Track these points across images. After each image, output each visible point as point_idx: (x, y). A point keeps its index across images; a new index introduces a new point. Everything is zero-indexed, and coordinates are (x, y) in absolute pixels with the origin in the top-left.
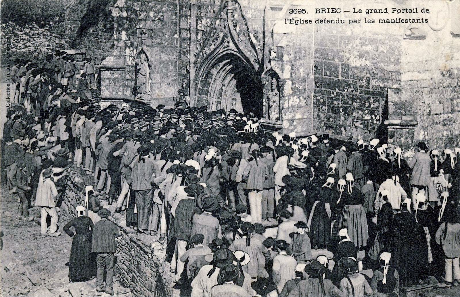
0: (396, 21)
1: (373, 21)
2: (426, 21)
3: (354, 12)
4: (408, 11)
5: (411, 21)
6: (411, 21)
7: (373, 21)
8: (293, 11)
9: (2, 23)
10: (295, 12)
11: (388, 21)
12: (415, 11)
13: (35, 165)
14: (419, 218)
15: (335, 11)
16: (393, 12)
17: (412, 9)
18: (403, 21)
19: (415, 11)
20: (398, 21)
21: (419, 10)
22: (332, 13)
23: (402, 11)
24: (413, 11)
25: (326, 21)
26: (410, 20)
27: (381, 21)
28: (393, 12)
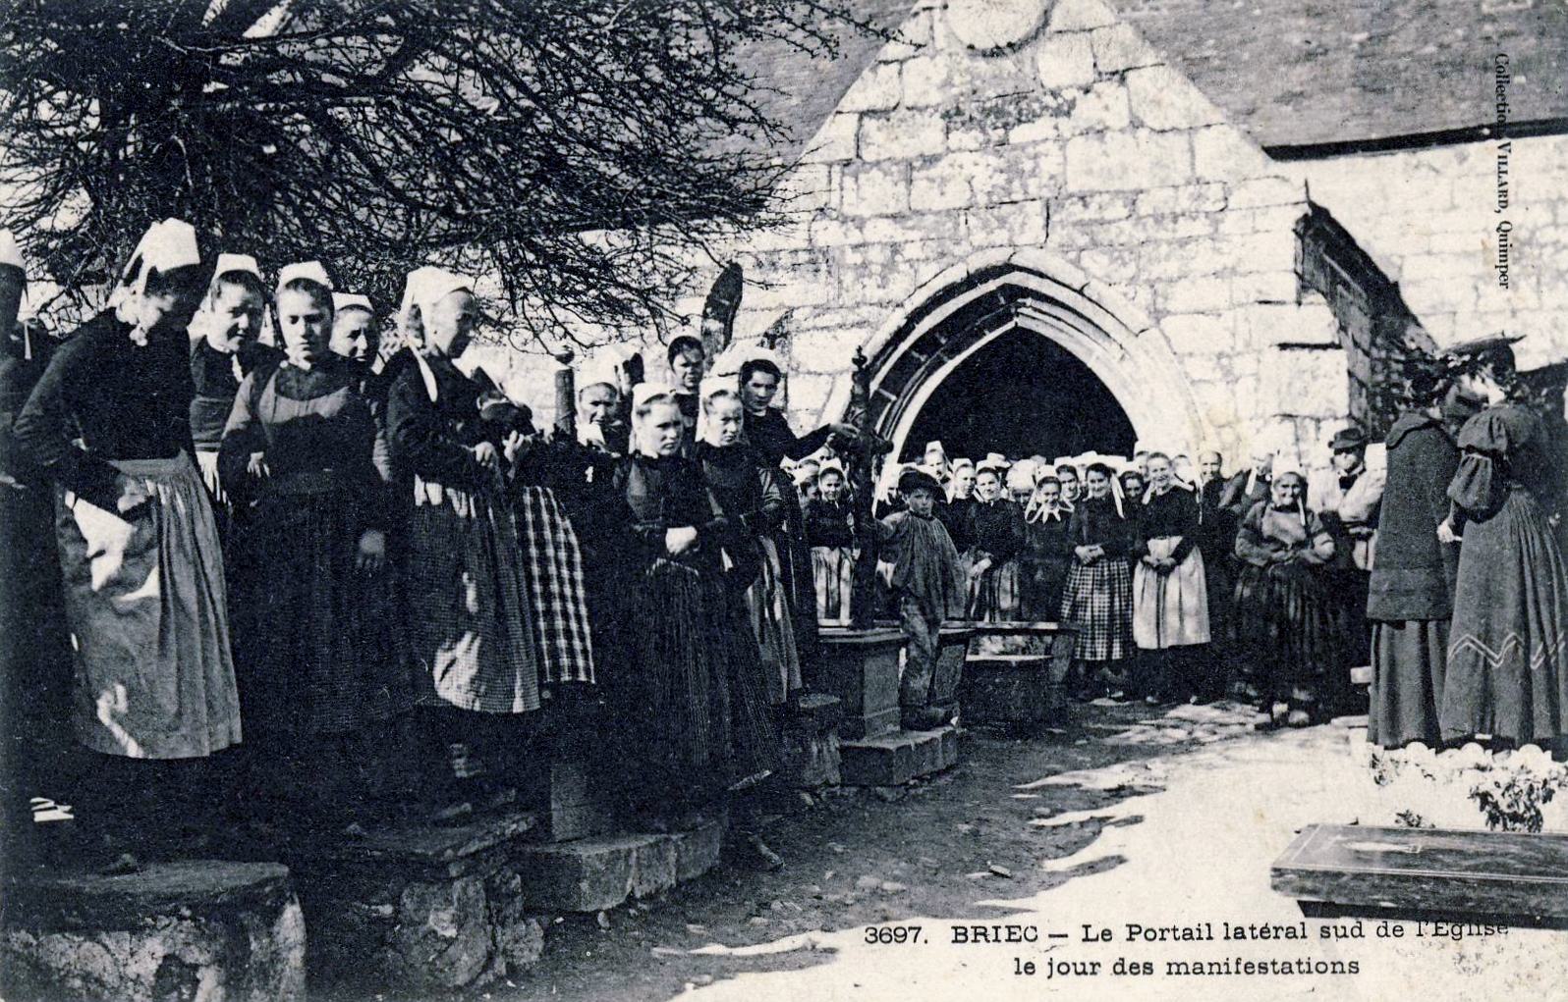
0: (1224, 969)
1: (1148, 968)
2: (1354, 967)
3: (1086, 939)
4: (1179, 934)
5: (1278, 967)
6: (1278, 967)
7: (1148, 968)
8: (1208, 925)
9: (7, 874)
10: (886, 938)
11: (1198, 969)
12: (1205, 935)
13: (89, 969)
14: (996, 354)
15: (1019, 934)
16: (1130, 939)
17: (1194, 927)
18: (1249, 966)
19: (1205, 935)
20: (1233, 969)
21: (1218, 931)
22: (1009, 940)
23: (1159, 935)
24: (1196, 934)
25: (1241, 968)
26: (1274, 963)
27: (1174, 968)
28: (1130, 939)
